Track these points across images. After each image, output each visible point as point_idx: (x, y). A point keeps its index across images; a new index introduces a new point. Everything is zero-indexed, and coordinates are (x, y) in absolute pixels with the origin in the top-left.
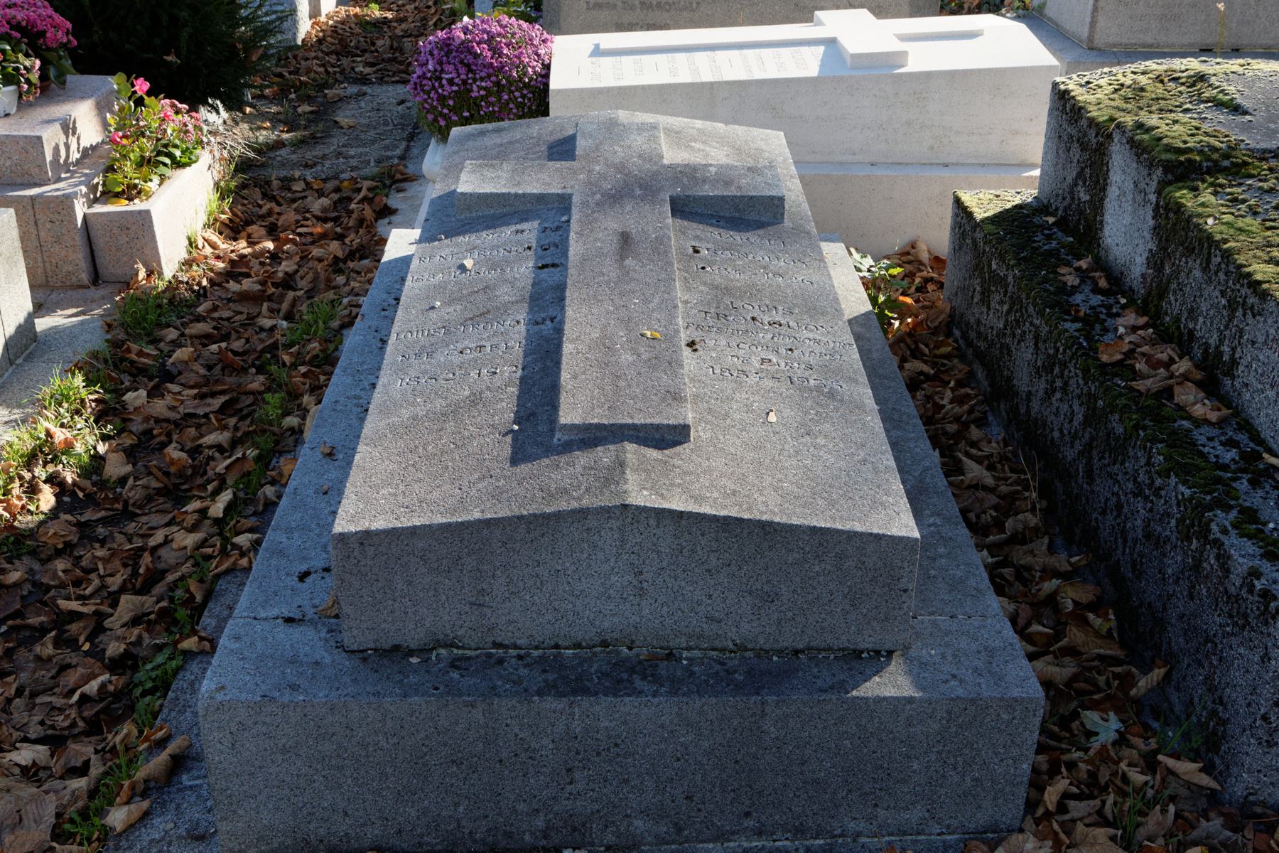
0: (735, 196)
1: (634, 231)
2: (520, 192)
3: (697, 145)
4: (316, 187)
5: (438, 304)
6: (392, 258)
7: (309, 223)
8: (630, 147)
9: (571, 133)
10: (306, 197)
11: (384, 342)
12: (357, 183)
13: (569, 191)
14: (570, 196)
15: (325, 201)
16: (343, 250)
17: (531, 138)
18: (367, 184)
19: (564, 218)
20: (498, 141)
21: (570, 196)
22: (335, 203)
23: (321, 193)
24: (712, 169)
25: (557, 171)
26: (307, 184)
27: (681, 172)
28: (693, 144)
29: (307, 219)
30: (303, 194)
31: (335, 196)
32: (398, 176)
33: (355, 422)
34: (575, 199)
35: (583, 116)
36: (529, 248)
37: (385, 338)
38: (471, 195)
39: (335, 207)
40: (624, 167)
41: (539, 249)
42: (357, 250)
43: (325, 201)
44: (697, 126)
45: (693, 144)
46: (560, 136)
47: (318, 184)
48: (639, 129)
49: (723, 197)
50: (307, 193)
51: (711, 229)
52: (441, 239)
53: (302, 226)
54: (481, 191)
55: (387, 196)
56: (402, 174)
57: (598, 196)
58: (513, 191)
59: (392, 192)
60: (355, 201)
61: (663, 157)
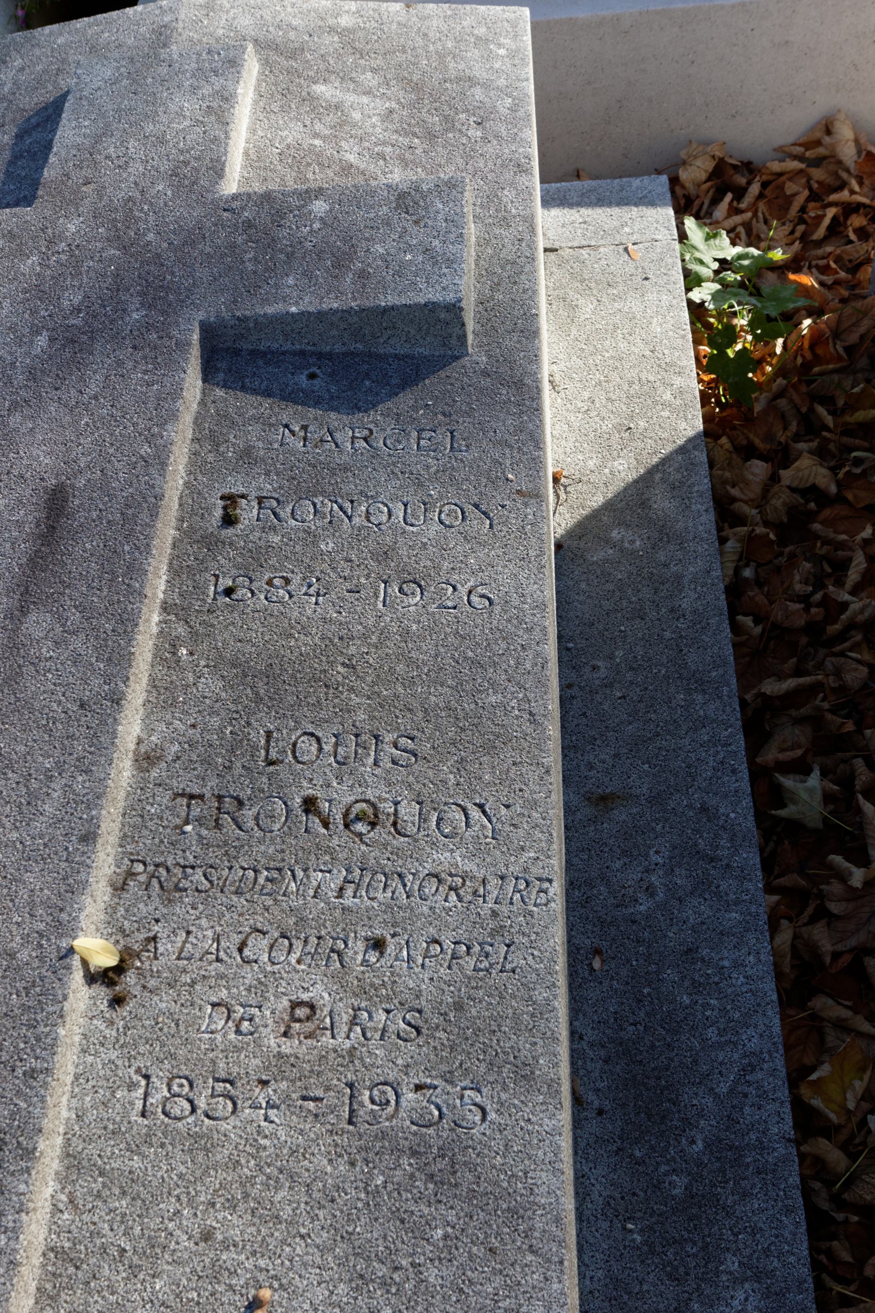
8: (162, 141)
40: (129, 217)
45: (319, 89)
49: (321, 316)
51: (287, 413)
57: (42, 341)
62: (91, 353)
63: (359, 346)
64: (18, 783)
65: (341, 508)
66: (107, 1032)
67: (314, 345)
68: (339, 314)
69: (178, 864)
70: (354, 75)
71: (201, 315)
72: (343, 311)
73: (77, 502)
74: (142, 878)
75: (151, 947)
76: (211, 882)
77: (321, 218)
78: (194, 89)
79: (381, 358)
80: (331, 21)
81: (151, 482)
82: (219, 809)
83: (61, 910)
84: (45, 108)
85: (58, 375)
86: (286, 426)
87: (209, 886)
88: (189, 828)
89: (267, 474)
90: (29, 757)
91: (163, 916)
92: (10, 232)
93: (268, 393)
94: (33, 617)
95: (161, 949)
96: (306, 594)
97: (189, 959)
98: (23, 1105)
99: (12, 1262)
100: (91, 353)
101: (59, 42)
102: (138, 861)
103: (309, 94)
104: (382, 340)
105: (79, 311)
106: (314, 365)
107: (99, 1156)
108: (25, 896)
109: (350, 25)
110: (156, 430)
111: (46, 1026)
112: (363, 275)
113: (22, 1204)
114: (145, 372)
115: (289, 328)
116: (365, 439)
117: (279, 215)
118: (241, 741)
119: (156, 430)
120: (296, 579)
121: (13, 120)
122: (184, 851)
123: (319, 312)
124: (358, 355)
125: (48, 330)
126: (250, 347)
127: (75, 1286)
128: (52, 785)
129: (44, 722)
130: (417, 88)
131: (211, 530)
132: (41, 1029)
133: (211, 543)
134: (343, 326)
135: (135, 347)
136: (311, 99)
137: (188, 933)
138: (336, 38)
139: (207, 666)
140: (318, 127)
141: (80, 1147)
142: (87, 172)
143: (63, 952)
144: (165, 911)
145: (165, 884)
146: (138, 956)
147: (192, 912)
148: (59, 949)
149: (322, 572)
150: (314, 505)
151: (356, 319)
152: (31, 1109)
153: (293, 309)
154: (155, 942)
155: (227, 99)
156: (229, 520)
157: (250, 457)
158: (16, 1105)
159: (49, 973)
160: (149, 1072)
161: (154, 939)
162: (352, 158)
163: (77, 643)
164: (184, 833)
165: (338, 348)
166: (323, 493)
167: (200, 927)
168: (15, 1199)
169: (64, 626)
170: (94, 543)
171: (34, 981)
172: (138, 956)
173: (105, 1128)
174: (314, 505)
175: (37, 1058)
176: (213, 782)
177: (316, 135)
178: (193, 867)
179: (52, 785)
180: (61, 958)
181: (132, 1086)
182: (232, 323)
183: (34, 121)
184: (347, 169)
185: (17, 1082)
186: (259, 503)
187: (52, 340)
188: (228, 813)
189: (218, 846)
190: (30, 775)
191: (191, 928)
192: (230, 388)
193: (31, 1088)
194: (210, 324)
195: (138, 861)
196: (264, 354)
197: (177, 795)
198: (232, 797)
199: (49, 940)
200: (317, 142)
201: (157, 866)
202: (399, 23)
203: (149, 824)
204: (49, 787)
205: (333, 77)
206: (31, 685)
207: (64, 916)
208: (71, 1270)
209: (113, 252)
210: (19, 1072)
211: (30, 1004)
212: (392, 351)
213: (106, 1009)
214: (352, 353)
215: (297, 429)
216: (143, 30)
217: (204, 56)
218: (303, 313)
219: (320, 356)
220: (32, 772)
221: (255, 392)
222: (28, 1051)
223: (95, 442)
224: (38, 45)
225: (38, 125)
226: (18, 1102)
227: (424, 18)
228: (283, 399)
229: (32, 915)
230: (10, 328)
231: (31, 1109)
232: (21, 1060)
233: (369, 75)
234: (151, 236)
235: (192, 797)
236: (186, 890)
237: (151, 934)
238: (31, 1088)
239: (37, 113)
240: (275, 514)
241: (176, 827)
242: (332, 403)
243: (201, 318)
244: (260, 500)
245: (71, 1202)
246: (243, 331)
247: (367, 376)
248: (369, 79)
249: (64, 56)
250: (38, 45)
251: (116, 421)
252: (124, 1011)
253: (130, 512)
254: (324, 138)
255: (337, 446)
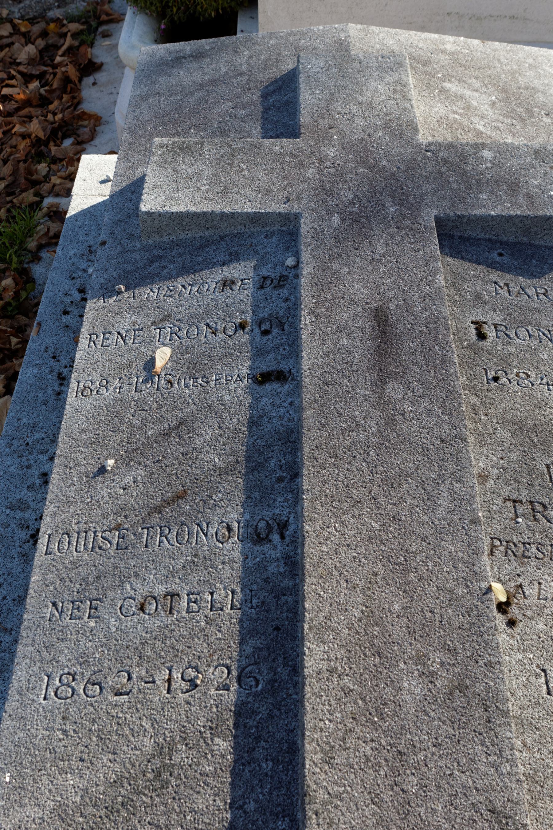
0: (526, 217)
1: (393, 306)
2: (228, 210)
3: (452, 87)
4: (23, 29)
5: (111, 462)
6: (79, 209)
7: (13, 82)
8: (370, 106)
9: (290, 67)
10: (13, 43)
11: (34, 537)
12: (64, 25)
13: (295, 208)
14: (297, 217)
15: (31, 49)
16: (44, 130)
17: (240, 74)
18: (74, 27)
19: (290, 262)
20: (197, 77)
21: (297, 217)
22: (41, 52)
23: (28, 39)
24: (487, 154)
25: (278, 158)
26: (14, 26)
27: (445, 161)
28: (447, 85)
29: (12, 77)
30: (9, 40)
31: (41, 43)
32: (104, 17)
33: (16, 565)
34: (305, 229)
35: (303, 34)
36: (242, 326)
37: (65, 372)
38: (160, 215)
39: (42, 57)
40: (366, 149)
41: (257, 331)
42: (60, 127)
43: (31, 49)
44: (449, 47)
45: (447, 85)
46: (275, 72)
47: (25, 26)
48: (379, 68)
49: (509, 218)
50: (14, 39)
51: (494, 275)
52: (119, 293)
53: (8, 86)
54: (174, 209)
55: (92, 45)
56: (108, 14)
57: (336, 219)
58: (217, 208)
59: (98, 37)
60: (60, 52)
61: (416, 129)
62: (371, 229)
63: (525, 239)
64: (417, 486)
65: (544, 334)
66: (511, 641)
67: (498, 236)
68: (521, 218)
69: (520, 541)
70: (464, 79)
71: (435, 212)
72: (523, 216)
73: (394, 318)
74: (502, 549)
75: (520, 591)
76: (542, 553)
77: (491, 161)
78: (381, 78)
79: (539, 247)
80: (442, 47)
81: (439, 309)
82: (533, 510)
83: (473, 565)
84: (276, 81)
85: (354, 241)
86: (495, 283)
87: (542, 556)
88: (520, 520)
89: (494, 310)
90: (419, 471)
91: (522, 572)
92: (291, 153)
93: (478, 262)
94: (390, 386)
95: (527, 593)
96: (541, 384)
97: (546, 599)
98: (492, 683)
99: (518, 780)
100: (371, 229)
101: (271, 42)
102: (495, 538)
103: (442, 88)
104: (539, 236)
105: (354, 204)
106: (500, 248)
107: (532, 718)
108: (447, 556)
109: (453, 50)
110: (430, 278)
111: (489, 635)
112: (529, 196)
113: (512, 745)
114: (411, 243)
115: (487, 224)
116: (544, 294)
117: (463, 157)
118: (533, 469)
119: (430, 278)
120: (533, 375)
121: (256, 87)
122: (521, 534)
123: (509, 216)
124: (523, 244)
125: (338, 213)
126: (459, 234)
127: (544, 798)
128: (440, 488)
129: (421, 450)
130: (504, 91)
131: (472, 342)
132: (486, 637)
133: (476, 351)
134: (520, 225)
135: (398, 228)
136: (443, 91)
137: (540, 583)
138: (447, 57)
139: (498, 423)
140: (455, 108)
141: (519, 713)
142: (329, 121)
143: (484, 591)
144: (522, 569)
145: (516, 553)
146: (514, 596)
147: (538, 571)
148: (480, 589)
149: (546, 371)
150: (528, 331)
151: (530, 222)
152: (497, 686)
153: (492, 213)
154: (522, 588)
155: (404, 86)
156: (482, 336)
157: (481, 300)
158: (486, 683)
159: (479, 603)
160: (545, 668)
161: (521, 586)
162: (481, 128)
163: (425, 402)
164: (518, 523)
165: (512, 239)
166: (531, 324)
167: (545, 580)
168: (507, 741)
169: (413, 392)
170: (415, 343)
171: (471, 608)
172: (514, 596)
173: (530, 701)
174: (528, 331)
175: (490, 655)
176: (524, 493)
177: (455, 112)
178: (529, 544)
179: (440, 488)
180: (484, 594)
181: (537, 676)
182: (454, 218)
183: (271, 88)
184: (479, 134)
185: (482, 669)
186: (495, 328)
187: (343, 220)
188: (539, 512)
189: (540, 532)
190: (423, 481)
191: (541, 581)
192: (455, 257)
193: (493, 673)
194: (440, 218)
195: (495, 538)
196: (468, 239)
197: (505, 500)
198: (538, 503)
199: (472, 583)
200: (456, 116)
201: (507, 542)
202: (481, 52)
203: (495, 516)
204: (439, 490)
205: (453, 80)
206: (404, 427)
207: (476, 568)
208: (539, 788)
209: (363, 170)
210: (481, 663)
211: (473, 621)
212: (543, 243)
213: (506, 628)
214: (520, 243)
215: (502, 285)
216: (328, 40)
217: (380, 59)
218: (498, 216)
219: (502, 243)
220: (424, 480)
221: (470, 261)
222: (483, 650)
223: (393, 283)
224: (257, 43)
225: (274, 91)
226: (487, 681)
227: (495, 50)
228: (488, 266)
229: (455, 567)
230: (313, 210)
231: (497, 686)
232: (480, 656)
233: (474, 80)
234: (384, 163)
235: (515, 501)
236: (530, 557)
237: (518, 583)
238: (493, 673)
239: (271, 84)
240: (506, 334)
241: (511, 519)
242: (517, 271)
243: (435, 214)
244: (495, 326)
245: (525, 746)
246: (459, 224)
247: (532, 257)
248: (477, 84)
249: (278, 51)
250: (257, 43)
251: (402, 271)
252: (517, 630)
253: (431, 326)
254: (460, 114)
255: (528, 296)
